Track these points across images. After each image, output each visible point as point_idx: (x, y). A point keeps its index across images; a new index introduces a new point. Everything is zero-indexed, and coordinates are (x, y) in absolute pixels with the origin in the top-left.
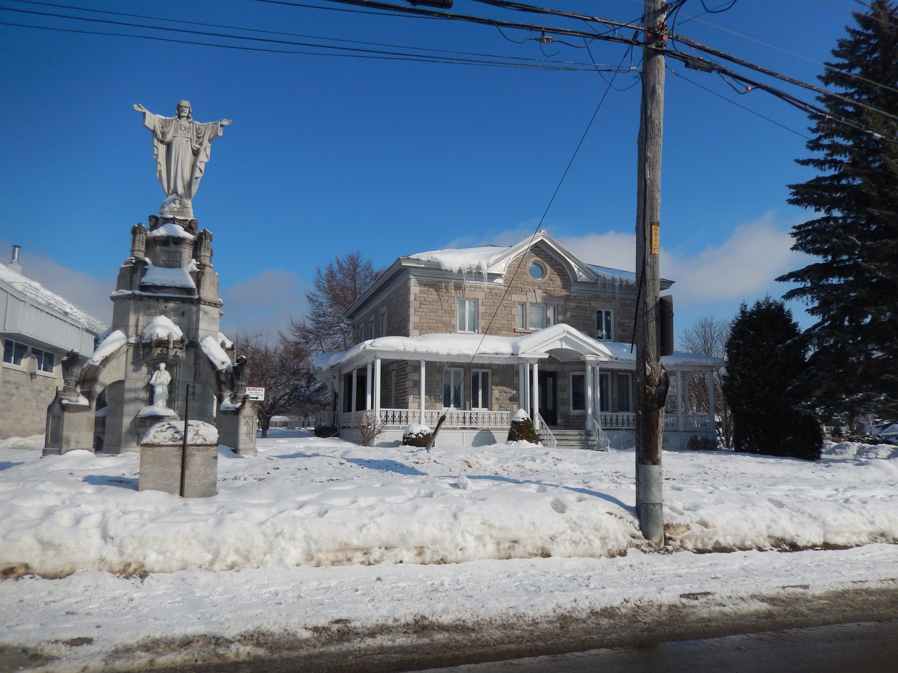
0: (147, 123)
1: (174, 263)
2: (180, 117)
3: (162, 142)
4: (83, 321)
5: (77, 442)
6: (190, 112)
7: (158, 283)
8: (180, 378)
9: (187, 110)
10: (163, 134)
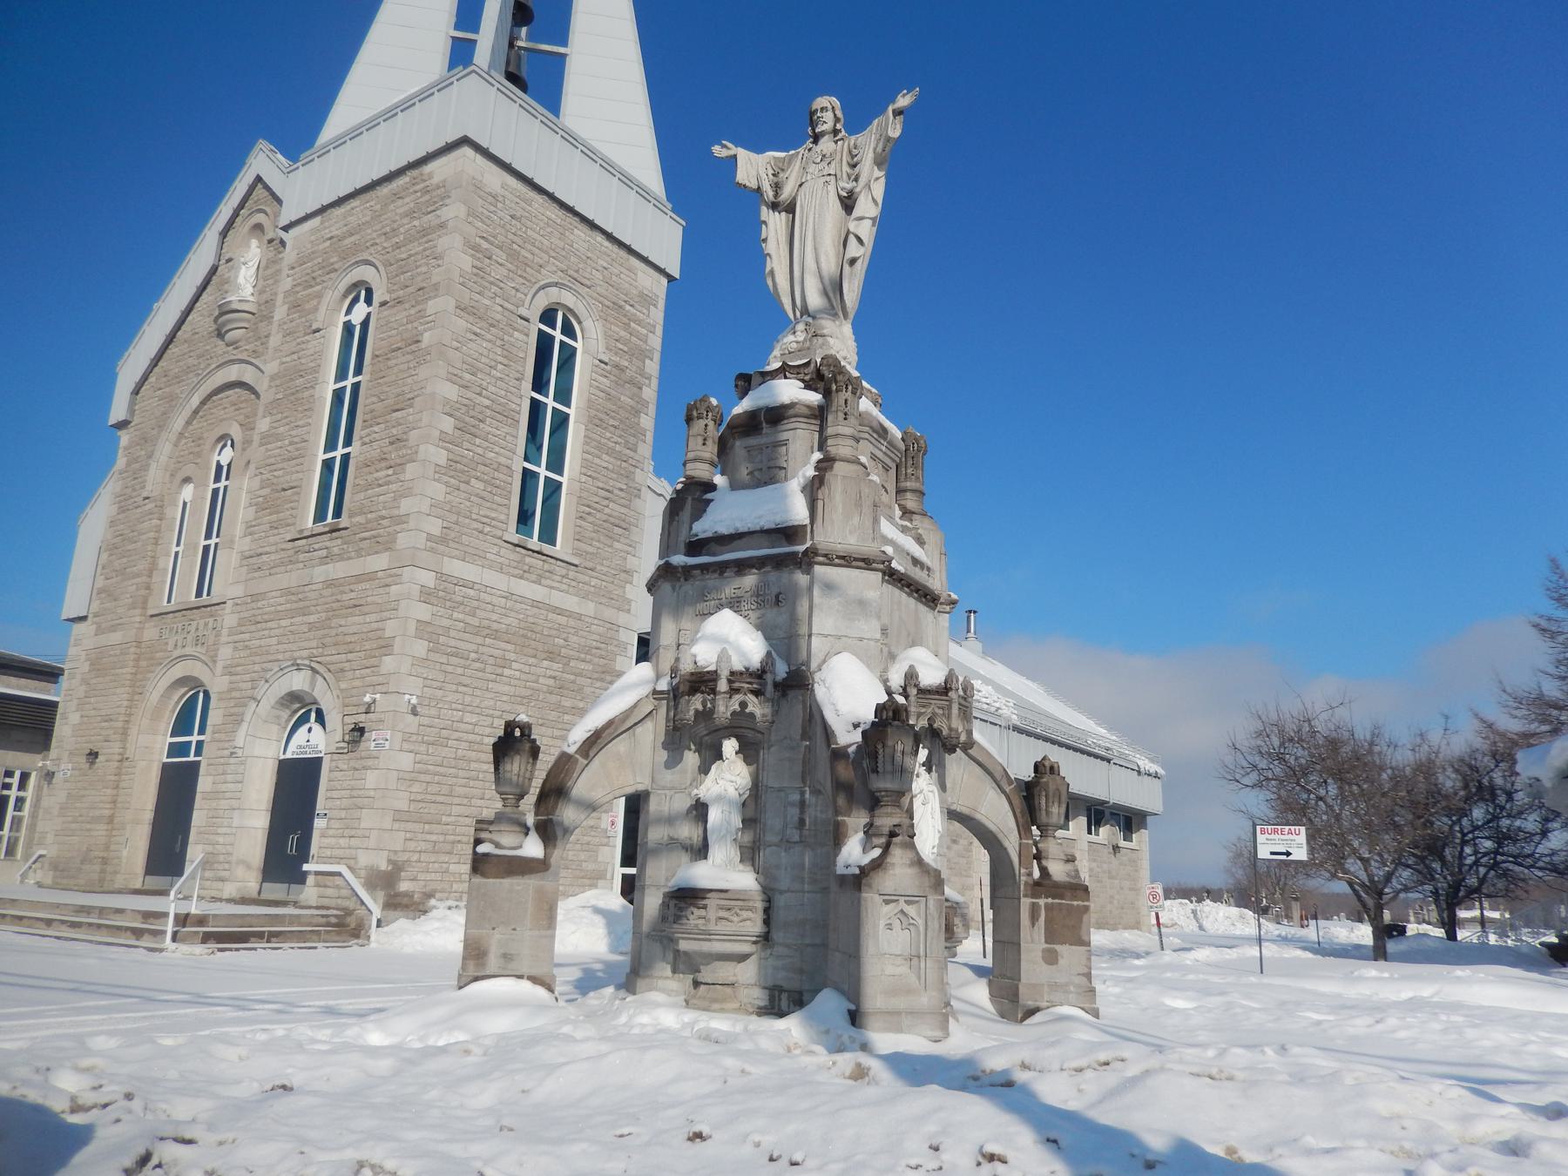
0: (741, 177)
1: (768, 474)
2: (816, 138)
3: (774, 206)
4: (1005, 712)
5: (507, 957)
6: (837, 120)
7: (724, 530)
8: (770, 780)
9: (828, 117)
10: (777, 187)
